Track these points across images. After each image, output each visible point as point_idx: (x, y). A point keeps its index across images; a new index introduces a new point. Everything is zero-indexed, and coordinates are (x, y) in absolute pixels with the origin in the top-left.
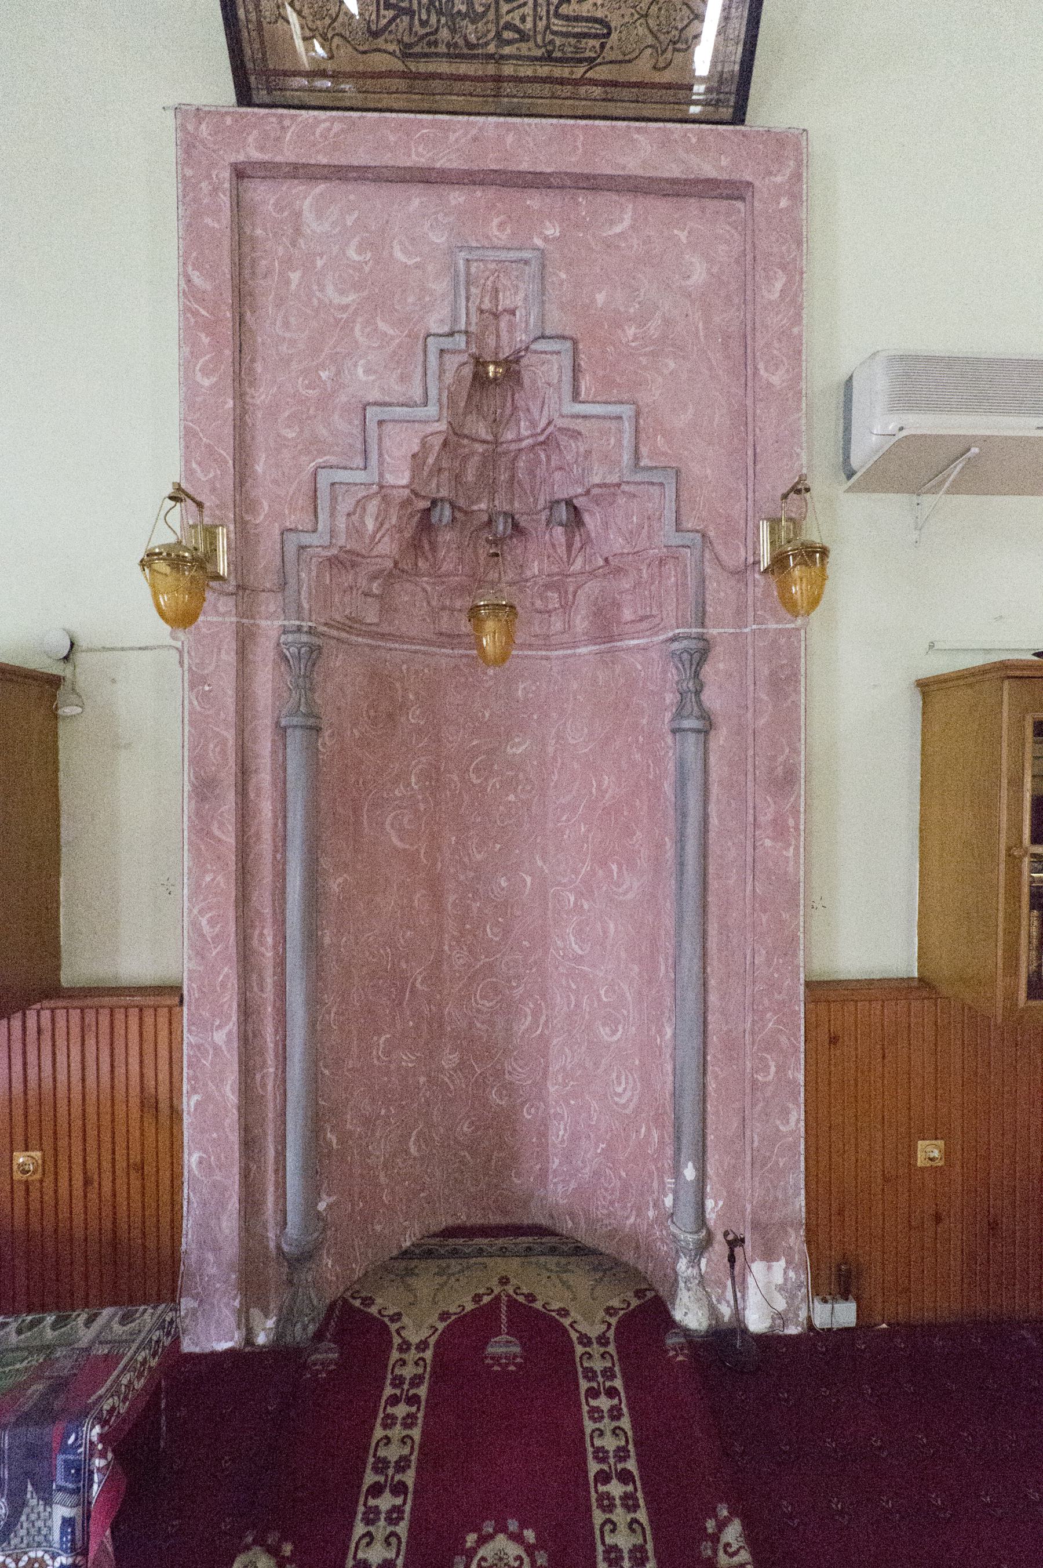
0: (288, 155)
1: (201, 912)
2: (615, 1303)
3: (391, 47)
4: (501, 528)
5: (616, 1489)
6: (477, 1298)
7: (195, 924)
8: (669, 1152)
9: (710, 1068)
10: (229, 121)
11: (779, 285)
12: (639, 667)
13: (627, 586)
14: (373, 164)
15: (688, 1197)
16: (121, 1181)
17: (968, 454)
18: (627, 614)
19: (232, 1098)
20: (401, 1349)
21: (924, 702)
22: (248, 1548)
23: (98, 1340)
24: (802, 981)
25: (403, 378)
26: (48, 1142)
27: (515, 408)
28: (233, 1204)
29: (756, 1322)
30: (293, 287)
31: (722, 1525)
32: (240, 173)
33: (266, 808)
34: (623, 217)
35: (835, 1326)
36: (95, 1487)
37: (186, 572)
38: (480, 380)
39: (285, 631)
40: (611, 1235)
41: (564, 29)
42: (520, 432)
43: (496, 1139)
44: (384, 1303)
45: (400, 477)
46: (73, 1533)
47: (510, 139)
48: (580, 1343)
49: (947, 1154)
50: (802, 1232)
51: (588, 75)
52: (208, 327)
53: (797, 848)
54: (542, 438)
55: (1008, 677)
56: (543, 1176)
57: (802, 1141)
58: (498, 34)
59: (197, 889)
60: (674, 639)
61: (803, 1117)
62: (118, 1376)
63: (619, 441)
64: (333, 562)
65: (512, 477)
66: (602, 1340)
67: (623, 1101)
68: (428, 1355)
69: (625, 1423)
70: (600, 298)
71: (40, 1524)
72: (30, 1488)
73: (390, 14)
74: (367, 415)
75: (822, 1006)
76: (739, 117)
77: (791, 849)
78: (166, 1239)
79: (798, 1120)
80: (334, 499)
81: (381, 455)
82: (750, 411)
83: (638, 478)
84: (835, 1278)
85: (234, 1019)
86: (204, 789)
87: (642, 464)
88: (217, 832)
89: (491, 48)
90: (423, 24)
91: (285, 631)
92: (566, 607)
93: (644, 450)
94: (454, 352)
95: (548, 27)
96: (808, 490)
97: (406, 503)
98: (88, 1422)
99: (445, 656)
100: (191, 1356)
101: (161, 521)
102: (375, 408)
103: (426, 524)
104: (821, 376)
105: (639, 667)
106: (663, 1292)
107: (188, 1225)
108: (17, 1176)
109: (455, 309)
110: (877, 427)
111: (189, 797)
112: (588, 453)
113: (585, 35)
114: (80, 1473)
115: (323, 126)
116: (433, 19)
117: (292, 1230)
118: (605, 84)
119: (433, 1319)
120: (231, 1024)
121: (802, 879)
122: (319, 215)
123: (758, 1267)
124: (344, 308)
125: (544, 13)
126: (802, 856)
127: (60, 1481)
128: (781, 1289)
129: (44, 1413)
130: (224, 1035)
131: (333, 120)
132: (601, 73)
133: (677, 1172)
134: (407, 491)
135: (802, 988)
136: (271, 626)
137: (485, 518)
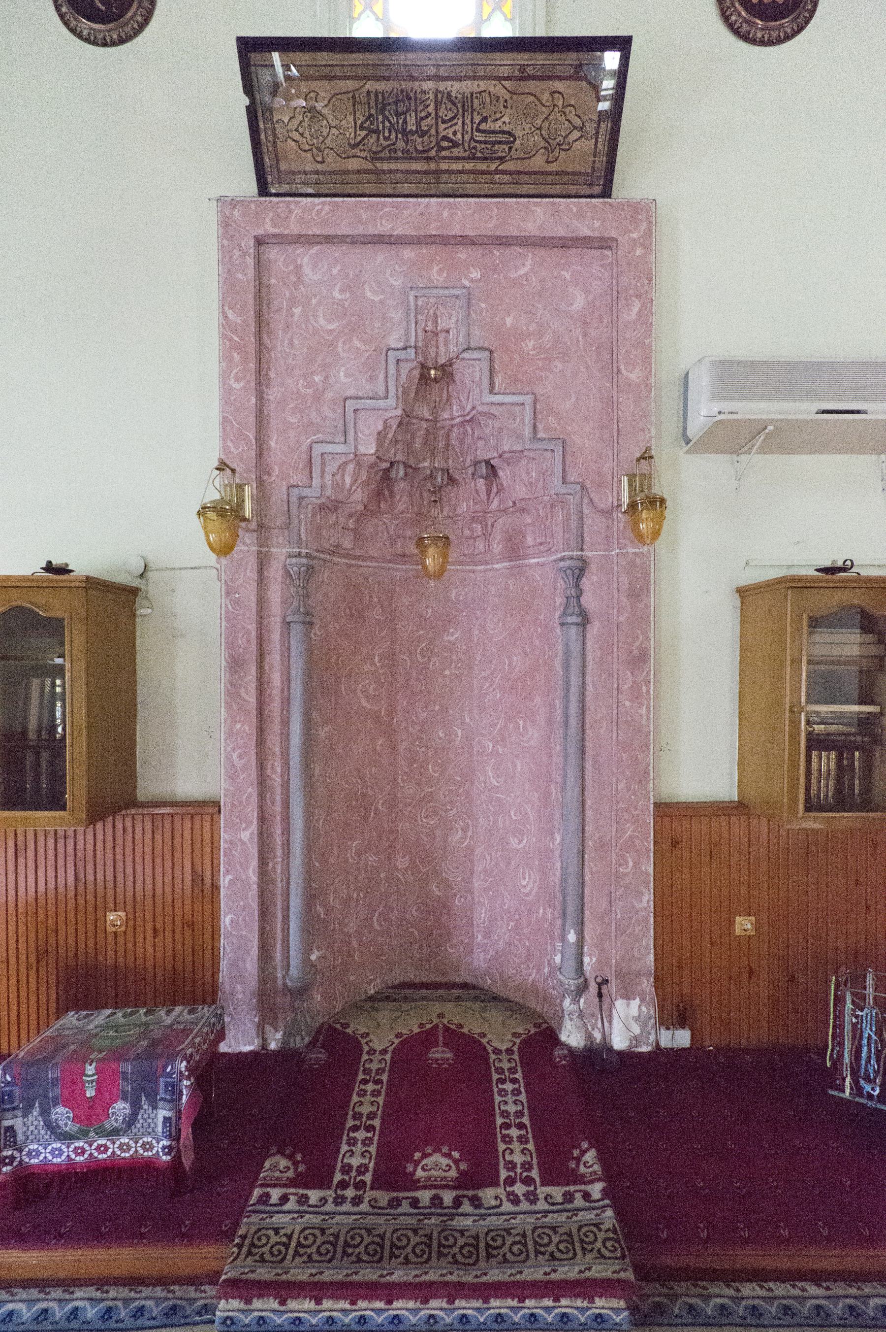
0: (294, 228)
1: (234, 750)
2: (520, 1030)
3: (364, 154)
4: (440, 480)
5: (514, 1132)
6: (421, 1025)
7: (229, 759)
8: (559, 923)
9: (586, 864)
10: (253, 206)
11: (635, 310)
12: (539, 578)
13: (529, 521)
14: (351, 233)
15: (571, 952)
16: (178, 936)
17: (767, 431)
18: (529, 541)
19: (254, 878)
20: (368, 1053)
21: (742, 603)
22: (274, 1155)
23: (176, 1021)
24: (652, 801)
25: (372, 379)
26: (129, 908)
27: (449, 396)
28: (255, 951)
29: (619, 1042)
30: (296, 318)
31: (583, 1153)
32: (260, 242)
33: (276, 679)
34: (526, 264)
35: (675, 1046)
36: (184, 1097)
37: (224, 514)
38: (424, 378)
39: (290, 556)
40: (518, 987)
41: (483, 139)
42: (453, 413)
43: (436, 920)
44: (357, 1026)
45: (369, 448)
46: (170, 1126)
47: (445, 213)
48: (494, 1052)
49: (757, 927)
50: (652, 980)
51: (500, 168)
52: (238, 348)
53: (648, 708)
54: (468, 418)
55: (792, 587)
56: (469, 950)
57: (652, 915)
58: (438, 143)
59: (230, 734)
60: (562, 559)
61: (652, 898)
62: (193, 1038)
63: (522, 421)
64: (322, 507)
65: (447, 445)
66: (509, 1051)
67: (527, 891)
68: (388, 1057)
69: (523, 1097)
70: (509, 321)
71: (150, 1121)
72: (144, 1098)
73: (364, 133)
74: (346, 406)
75: (667, 820)
76: (606, 193)
77: (644, 708)
78: (208, 974)
79: (649, 901)
80: (323, 464)
81: (356, 433)
82: (615, 399)
83: (537, 445)
84: (674, 1012)
85: (255, 823)
86: (235, 664)
87: (538, 436)
88: (243, 695)
89: (433, 153)
90: (385, 139)
91: (290, 556)
92: (486, 536)
93: (540, 427)
94: (407, 360)
95: (472, 138)
96: (651, 457)
97: (372, 466)
98: (179, 1059)
99: (402, 570)
100: (225, 1055)
101: (211, 485)
102: (352, 401)
103: (386, 477)
104: (667, 371)
105: (539, 578)
106: (553, 1024)
107: (224, 965)
108: (110, 929)
109: (407, 334)
110: (704, 411)
111: (225, 670)
112: (500, 430)
113: (500, 142)
114: (174, 1090)
115: (317, 208)
116: (393, 136)
117: (294, 972)
118: (510, 173)
119: (391, 1037)
120: (253, 826)
121: (652, 729)
122: (314, 268)
123: (620, 1004)
124: (331, 332)
125: (469, 130)
126: (652, 713)
127: (162, 1094)
128: (636, 1019)
129: (150, 1054)
130: (248, 835)
131: (323, 203)
132: (510, 166)
133: (563, 939)
134: (374, 457)
135: (652, 806)
136: (280, 552)
137: (428, 472)
